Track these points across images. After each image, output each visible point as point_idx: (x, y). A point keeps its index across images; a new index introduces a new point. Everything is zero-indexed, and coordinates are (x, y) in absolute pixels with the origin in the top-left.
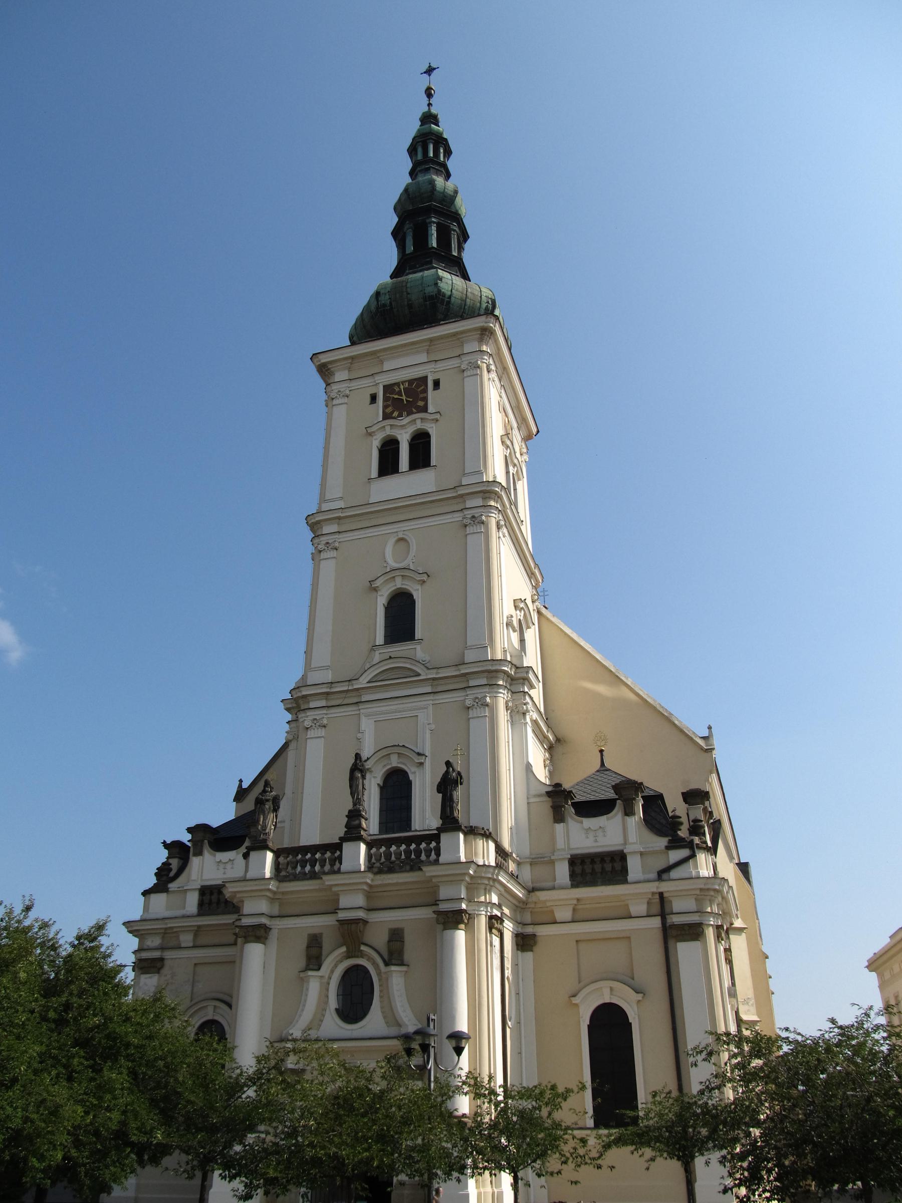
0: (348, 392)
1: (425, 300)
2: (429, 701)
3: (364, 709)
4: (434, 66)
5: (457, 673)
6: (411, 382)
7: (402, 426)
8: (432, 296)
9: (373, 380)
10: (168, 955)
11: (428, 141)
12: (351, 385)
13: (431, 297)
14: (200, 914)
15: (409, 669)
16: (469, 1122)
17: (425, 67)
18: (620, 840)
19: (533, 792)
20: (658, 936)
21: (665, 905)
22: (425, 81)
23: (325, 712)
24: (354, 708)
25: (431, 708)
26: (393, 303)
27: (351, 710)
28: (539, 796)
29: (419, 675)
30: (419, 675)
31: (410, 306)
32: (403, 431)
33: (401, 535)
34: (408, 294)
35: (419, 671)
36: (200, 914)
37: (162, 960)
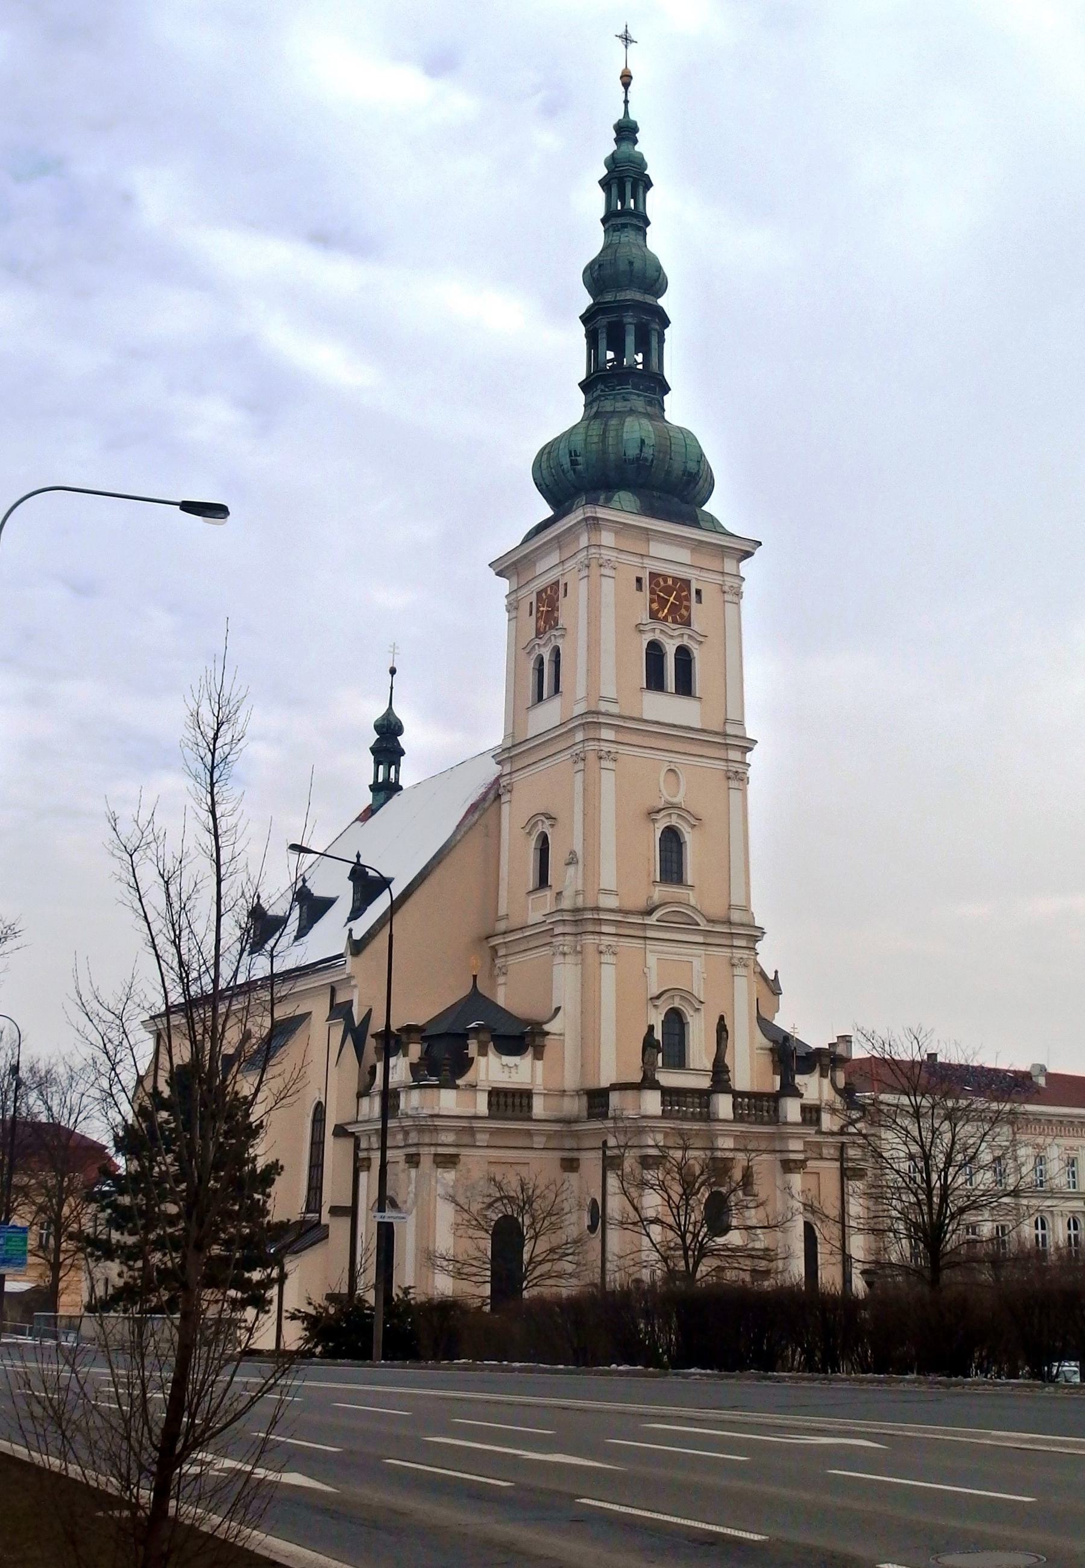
0: (617, 564)
1: (684, 475)
2: (699, 951)
3: (651, 946)
4: (621, 32)
5: (729, 931)
6: (675, 579)
7: (672, 637)
8: (692, 473)
9: (641, 561)
10: (463, 1151)
11: (625, 179)
12: (619, 556)
13: (690, 474)
14: (490, 1117)
15: (689, 915)
16: (92, 1236)
17: (620, 43)
18: (816, 1096)
19: (757, 1045)
20: (837, 1175)
21: (635, 1091)
22: (615, 59)
23: (615, 939)
24: (642, 942)
25: (703, 957)
26: (655, 462)
27: (637, 943)
28: (761, 1049)
29: (699, 925)
30: (699, 925)
31: (668, 473)
32: (671, 641)
33: (673, 768)
34: (671, 459)
35: (699, 922)
36: (490, 1117)
37: (457, 1156)
